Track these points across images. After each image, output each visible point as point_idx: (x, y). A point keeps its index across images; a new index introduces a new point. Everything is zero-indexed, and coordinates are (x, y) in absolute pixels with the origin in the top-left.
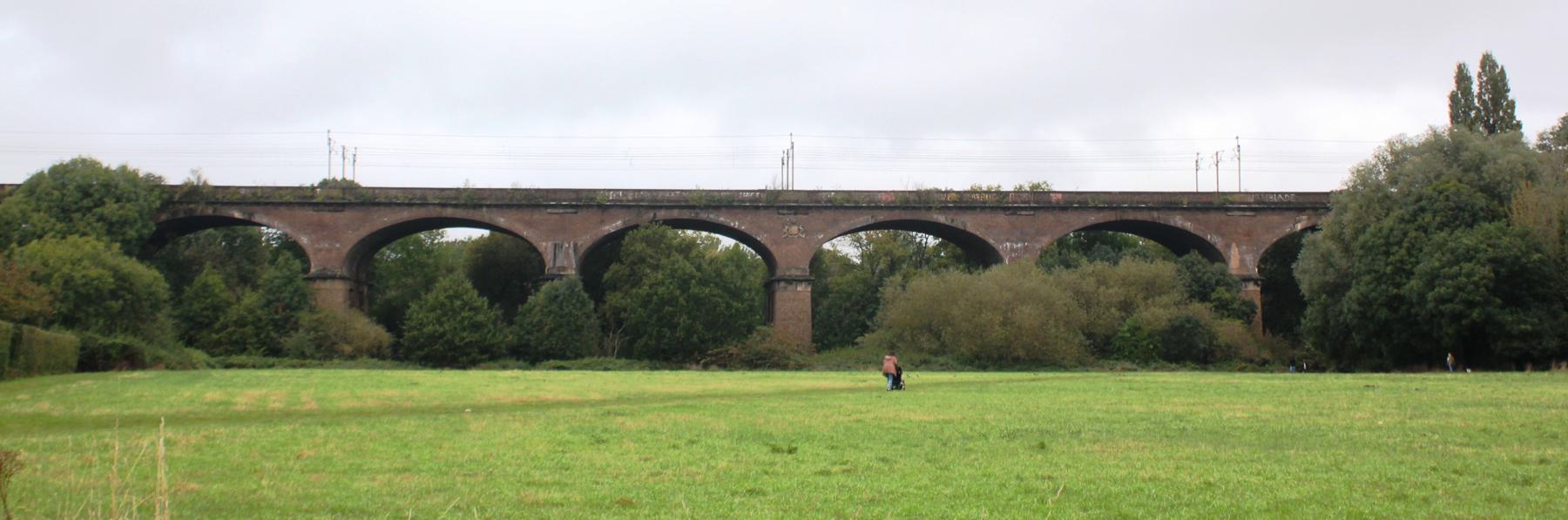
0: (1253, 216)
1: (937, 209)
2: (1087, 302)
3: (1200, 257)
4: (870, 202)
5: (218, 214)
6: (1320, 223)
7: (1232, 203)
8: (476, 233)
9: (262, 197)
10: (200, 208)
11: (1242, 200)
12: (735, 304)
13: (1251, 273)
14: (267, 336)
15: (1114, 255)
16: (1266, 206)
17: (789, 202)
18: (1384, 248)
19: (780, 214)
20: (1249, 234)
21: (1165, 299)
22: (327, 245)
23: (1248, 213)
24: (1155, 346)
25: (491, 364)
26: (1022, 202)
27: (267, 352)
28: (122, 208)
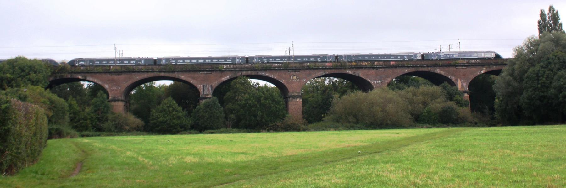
0: (466, 68)
1: (348, 68)
2: (411, 102)
3: (448, 84)
4: (323, 66)
5: (72, 77)
6: (503, 69)
7: (458, 64)
8: (168, 83)
9: (89, 70)
10: (66, 75)
11: (462, 63)
12: (278, 106)
13: (466, 90)
14: (95, 124)
15: (416, 84)
16: (470, 65)
17: (292, 67)
18: (536, 78)
19: (289, 72)
20: (464, 75)
21: (439, 100)
22: (115, 88)
23: (464, 67)
24: (437, 118)
25: (185, 132)
26: (380, 65)
27: (96, 130)
28: (37, 75)
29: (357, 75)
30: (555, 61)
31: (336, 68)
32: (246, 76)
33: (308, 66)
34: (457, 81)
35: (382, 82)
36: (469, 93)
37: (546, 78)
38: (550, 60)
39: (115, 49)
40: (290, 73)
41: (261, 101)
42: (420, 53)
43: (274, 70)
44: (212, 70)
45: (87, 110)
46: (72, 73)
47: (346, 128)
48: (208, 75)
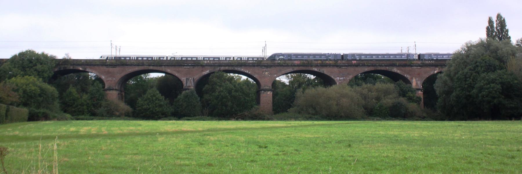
2: (365, 97)
3: (403, 82)
4: (292, 64)
5: (74, 68)
7: (413, 64)
8: (160, 75)
12: (247, 98)
14: (91, 109)
16: (424, 65)
18: (464, 79)
20: (419, 74)
21: (391, 96)
22: (111, 79)
24: (388, 112)
25: (166, 118)
26: (343, 64)
28: (42, 67)
29: (322, 72)
30: (482, 65)
31: (303, 65)
32: (222, 71)
33: (279, 64)
34: (412, 80)
35: (344, 79)
36: (422, 91)
37: (473, 79)
38: (478, 64)
39: (111, 45)
40: (262, 69)
41: (232, 93)
42: (416, 54)
43: (248, 66)
44: (195, 65)
45: (85, 97)
46: (74, 65)
47: (305, 119)
48: (191, 69)
